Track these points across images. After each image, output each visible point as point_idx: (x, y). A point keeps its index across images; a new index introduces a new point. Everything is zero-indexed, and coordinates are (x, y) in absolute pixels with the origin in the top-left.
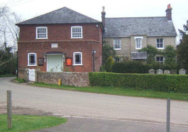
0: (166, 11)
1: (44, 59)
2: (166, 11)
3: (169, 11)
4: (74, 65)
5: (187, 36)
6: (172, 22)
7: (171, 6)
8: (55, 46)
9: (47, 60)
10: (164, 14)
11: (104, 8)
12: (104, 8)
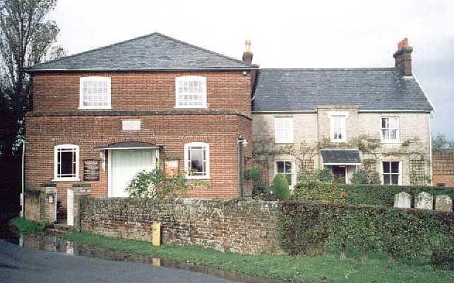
0: (396, 56)
1: (99, 161)
2: (396, 56)
3: (403, 55)
4: (208, 176)
5: (2, 238)
6: (414, 80)
7: (410, 44)
8: (131, 125)
9: (26, 202)
10: (391, 63)
11: (248, 43)
12: (248, 43)
